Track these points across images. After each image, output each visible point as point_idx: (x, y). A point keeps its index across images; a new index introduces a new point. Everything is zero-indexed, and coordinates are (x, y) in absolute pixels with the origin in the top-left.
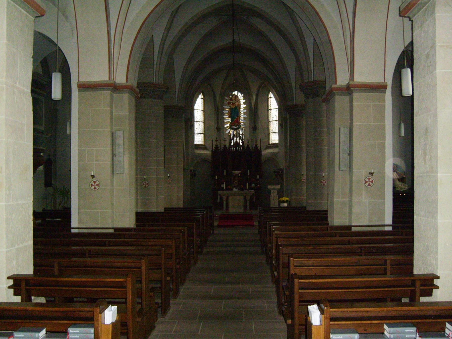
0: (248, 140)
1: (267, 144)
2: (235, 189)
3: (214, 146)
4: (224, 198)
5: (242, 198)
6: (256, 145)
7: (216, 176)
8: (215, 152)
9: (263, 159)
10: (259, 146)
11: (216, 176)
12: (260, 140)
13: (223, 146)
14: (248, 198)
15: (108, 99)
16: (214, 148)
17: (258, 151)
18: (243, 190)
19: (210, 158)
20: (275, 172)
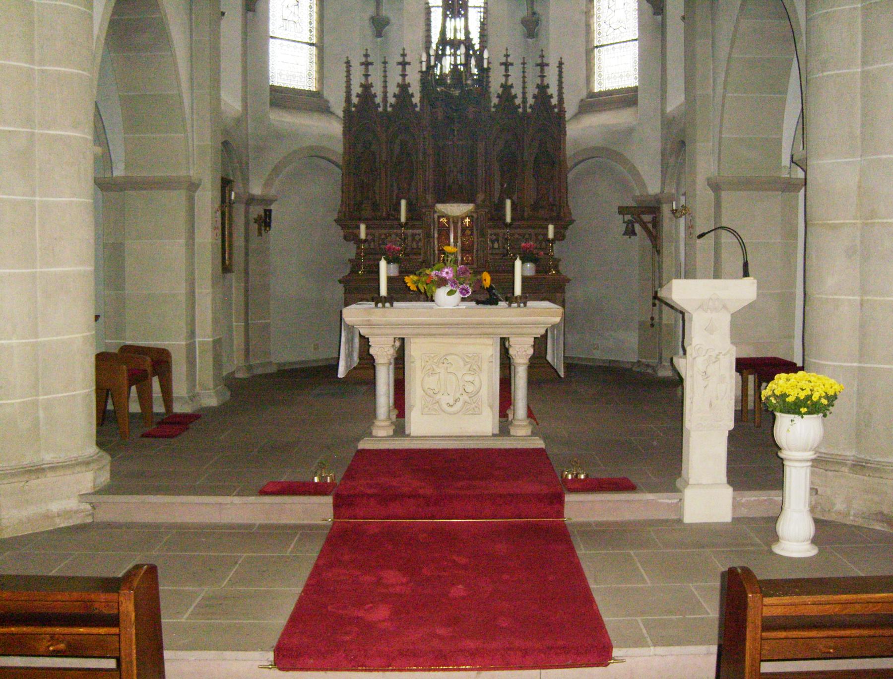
0: (507, 65)
1: (584, 94)
2: (441, 294)
3: (356, 89)
4: (382, 352)
5: (490, 352)
6: (542, 88)
7: (363, 227)
8: (361, 115)
9: (570, 149)
10: (553, 90)
11: (363, 227)
12: (561, 64)
13: (393, 89)
14: (522, 352)
15: (786, 542)
16: (355, 100)
17: (548, 117)
18: (492, 301)
19: (339, 148)
20: (622, 210)
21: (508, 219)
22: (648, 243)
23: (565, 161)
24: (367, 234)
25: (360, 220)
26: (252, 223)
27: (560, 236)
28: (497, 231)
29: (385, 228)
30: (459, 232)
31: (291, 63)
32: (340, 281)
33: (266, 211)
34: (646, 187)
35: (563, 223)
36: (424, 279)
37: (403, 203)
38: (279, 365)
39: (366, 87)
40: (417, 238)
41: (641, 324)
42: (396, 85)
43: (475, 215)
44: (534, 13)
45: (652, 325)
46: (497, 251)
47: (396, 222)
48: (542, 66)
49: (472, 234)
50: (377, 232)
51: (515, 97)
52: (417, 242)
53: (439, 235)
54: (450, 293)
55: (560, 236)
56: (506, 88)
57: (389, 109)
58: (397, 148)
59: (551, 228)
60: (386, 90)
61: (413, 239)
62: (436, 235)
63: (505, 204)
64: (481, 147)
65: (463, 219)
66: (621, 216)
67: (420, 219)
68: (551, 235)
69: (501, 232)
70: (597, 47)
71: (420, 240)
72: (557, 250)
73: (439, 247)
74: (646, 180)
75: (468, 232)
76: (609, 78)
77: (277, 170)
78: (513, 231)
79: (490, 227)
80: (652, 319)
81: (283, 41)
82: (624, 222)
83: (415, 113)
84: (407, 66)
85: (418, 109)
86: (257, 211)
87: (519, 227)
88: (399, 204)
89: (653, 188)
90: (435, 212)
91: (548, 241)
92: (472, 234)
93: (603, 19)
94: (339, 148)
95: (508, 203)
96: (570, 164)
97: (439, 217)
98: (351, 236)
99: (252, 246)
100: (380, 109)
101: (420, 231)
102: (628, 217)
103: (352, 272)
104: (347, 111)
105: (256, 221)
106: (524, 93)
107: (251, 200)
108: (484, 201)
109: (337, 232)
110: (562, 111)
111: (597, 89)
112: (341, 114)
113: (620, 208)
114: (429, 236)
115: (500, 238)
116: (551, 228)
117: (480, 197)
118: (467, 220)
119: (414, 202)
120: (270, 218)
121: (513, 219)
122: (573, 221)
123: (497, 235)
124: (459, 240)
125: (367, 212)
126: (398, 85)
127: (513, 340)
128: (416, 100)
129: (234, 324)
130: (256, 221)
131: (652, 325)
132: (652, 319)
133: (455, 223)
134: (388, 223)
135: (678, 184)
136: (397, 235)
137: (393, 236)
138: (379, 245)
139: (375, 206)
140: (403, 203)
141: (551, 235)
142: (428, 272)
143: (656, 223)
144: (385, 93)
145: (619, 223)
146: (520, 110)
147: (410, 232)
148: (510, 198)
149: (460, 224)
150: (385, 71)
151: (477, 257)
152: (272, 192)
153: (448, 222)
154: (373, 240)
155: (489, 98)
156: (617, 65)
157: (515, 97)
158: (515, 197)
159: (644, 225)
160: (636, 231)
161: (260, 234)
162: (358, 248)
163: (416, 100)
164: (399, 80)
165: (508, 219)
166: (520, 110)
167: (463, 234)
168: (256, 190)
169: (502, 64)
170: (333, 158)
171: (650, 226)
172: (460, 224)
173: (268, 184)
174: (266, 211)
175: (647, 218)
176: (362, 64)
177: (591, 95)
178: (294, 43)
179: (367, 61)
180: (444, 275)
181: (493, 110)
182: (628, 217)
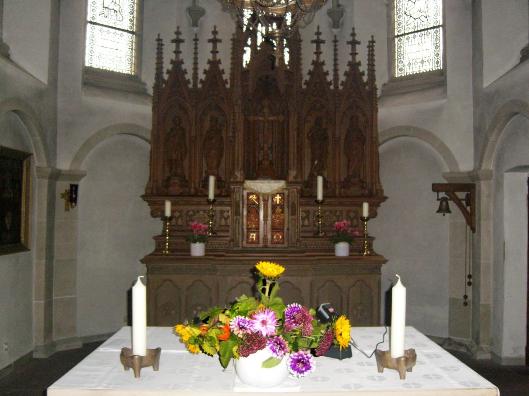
3: (167, 66)
6: (354, 65)
10: (364, 68)
12: (372, 42)
16: (166, 77)
19: (148, 125)
20: (436, 188)
21: (320, 197)
22: (462, 220)
23: (377, 138)
24: (173, 211)
25: (167, 196)
26: (58, 196)
27: (373, 214)
28: (308, 208)
29: (192, 205)
30: (270, 209)
31: (110, 49)
32: (142, 261)
33: (72, 186)
34: (458, 166)
35: (376, 198)
36: (213, 333)
37: (212, 180)
38: (85, 338)
39: (177, 64)
40: (225, 215)
41: (453, 302)
42: (206, 61)
43: (286, 192)
44: (339, 6)
45: (466, 304)
46: (309, 229)
47: (203, 199)
48: (354, 43)
49: (283, 212)
50: (185, 208)
51: (327, 73)
52: (226, 219)
53: (248, 212)
54: (268, 363)
55: (373, 214)
56: (318, 64)
57: (200, 86)
58: (207, 125)
59: (366, 206)
60: (196, 67)
61: (222, 216)
62: (245, 213)
63: (316, 180)
64: (293, 122)
65: (274, 196)
66: (436, 193)
67: (228, 196)
68: (366, 213)
69: (311, 209)
70: (398, 36)
71: (228, 216)
72: (372, 228)
73: (248, 225)
74: (457, 157)
75: (279, 210)
76: (410, 64)
77: (88, 145)
78: (325, 208)
79: (301, 205)
80: (466, 297)
81: (103, 28)
82: (438, 199)
83: (226, 89)
84: (218, 44)
85: (228, 86)
86: (63, 186)
87: (330, 204)
88: (207, 180)
89: (466, 165)
90: (244, 189)
91: (363, 219)
92: (283, 212)
93: (403, 10)
94: (149, 126)
95: (320, 179)
96: (380, 140)
97: (249, 194)
98: (157, 212)
99: (58, 221)
100: (190, 86)
101: (228, 208)
102: (442, 195)
103: (156, 250)
104: (156, 87)
105: (63, 196)
106: (336, 70)
107: (56, 176)
108: (296, 177)
109: (146, 208)
110: (374, 89)
111: (397, 74)
112: (151, 91)
113: (433, 185)
114: (237, 213)
115: (311, 216)
116: (366, 206)
117: (293, 173)
118: (278, 197)
119: (223, 179)
120: (76, 194)
121: (324, 196)
122: (386, 198)
123: (307, 212)
124: (269, 218)
125: (175, 189)
126: (209, 62)
127: (161, 34)
128: (226, 76)
129: (34, 302)
130: (63, 196)
131: (466, 304)
132: (466, 297)
133: (266, 201)
134: (196, 199)
135: (302, 177)
136: (204, 211)
137: (201, 213)
138: (187, 221)
139: (185, 183)
140: (212, 180)
141: (366, 213)
142: (222, 318)
143: (470, 200)
144: (196, 69)
145: (432, 201)
146: (332, 87)
147: (219, 208)
148: (321, 175)
149: (270, 201)
150: (196, 48)
151: (288, 234)
152: (83, 167)
153: (258, 199)
154: (180, 216)
155: (301, 75)
156: (418, 54)
157: (327, 73)
158: (325, 175)
159: (458, 202)
160: (451, 208)
161: (67, 209)
162: (165, 225)
163: (226, 76)
164: (210, 57)
165: (320, 197)
166: (332, 87)
167: (273, 212)
168: (64, 164)
169: (313, 42)
170: (144, 135)
171: (464, 203)
172: (270, 201)
173: (77, 159)
174: (72, 186)
175: (461, 195)
176: (173, 41)
177: (393, 79)
178: (114, 30)
179: (178, 38)
180: (257, 326)
181: (304, 87)
182: (442, 195)
